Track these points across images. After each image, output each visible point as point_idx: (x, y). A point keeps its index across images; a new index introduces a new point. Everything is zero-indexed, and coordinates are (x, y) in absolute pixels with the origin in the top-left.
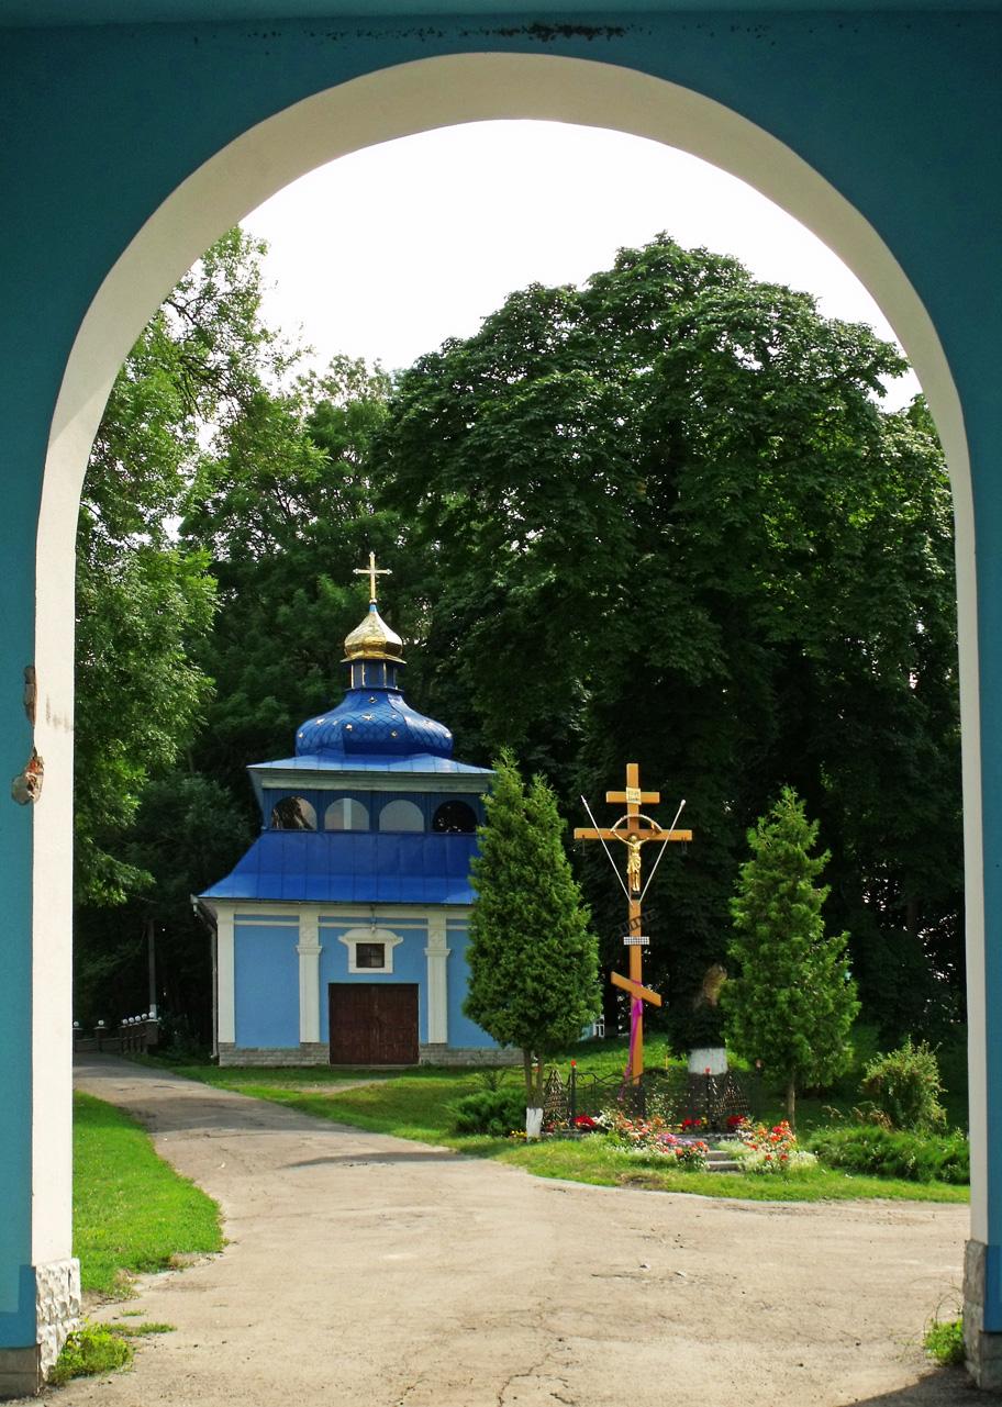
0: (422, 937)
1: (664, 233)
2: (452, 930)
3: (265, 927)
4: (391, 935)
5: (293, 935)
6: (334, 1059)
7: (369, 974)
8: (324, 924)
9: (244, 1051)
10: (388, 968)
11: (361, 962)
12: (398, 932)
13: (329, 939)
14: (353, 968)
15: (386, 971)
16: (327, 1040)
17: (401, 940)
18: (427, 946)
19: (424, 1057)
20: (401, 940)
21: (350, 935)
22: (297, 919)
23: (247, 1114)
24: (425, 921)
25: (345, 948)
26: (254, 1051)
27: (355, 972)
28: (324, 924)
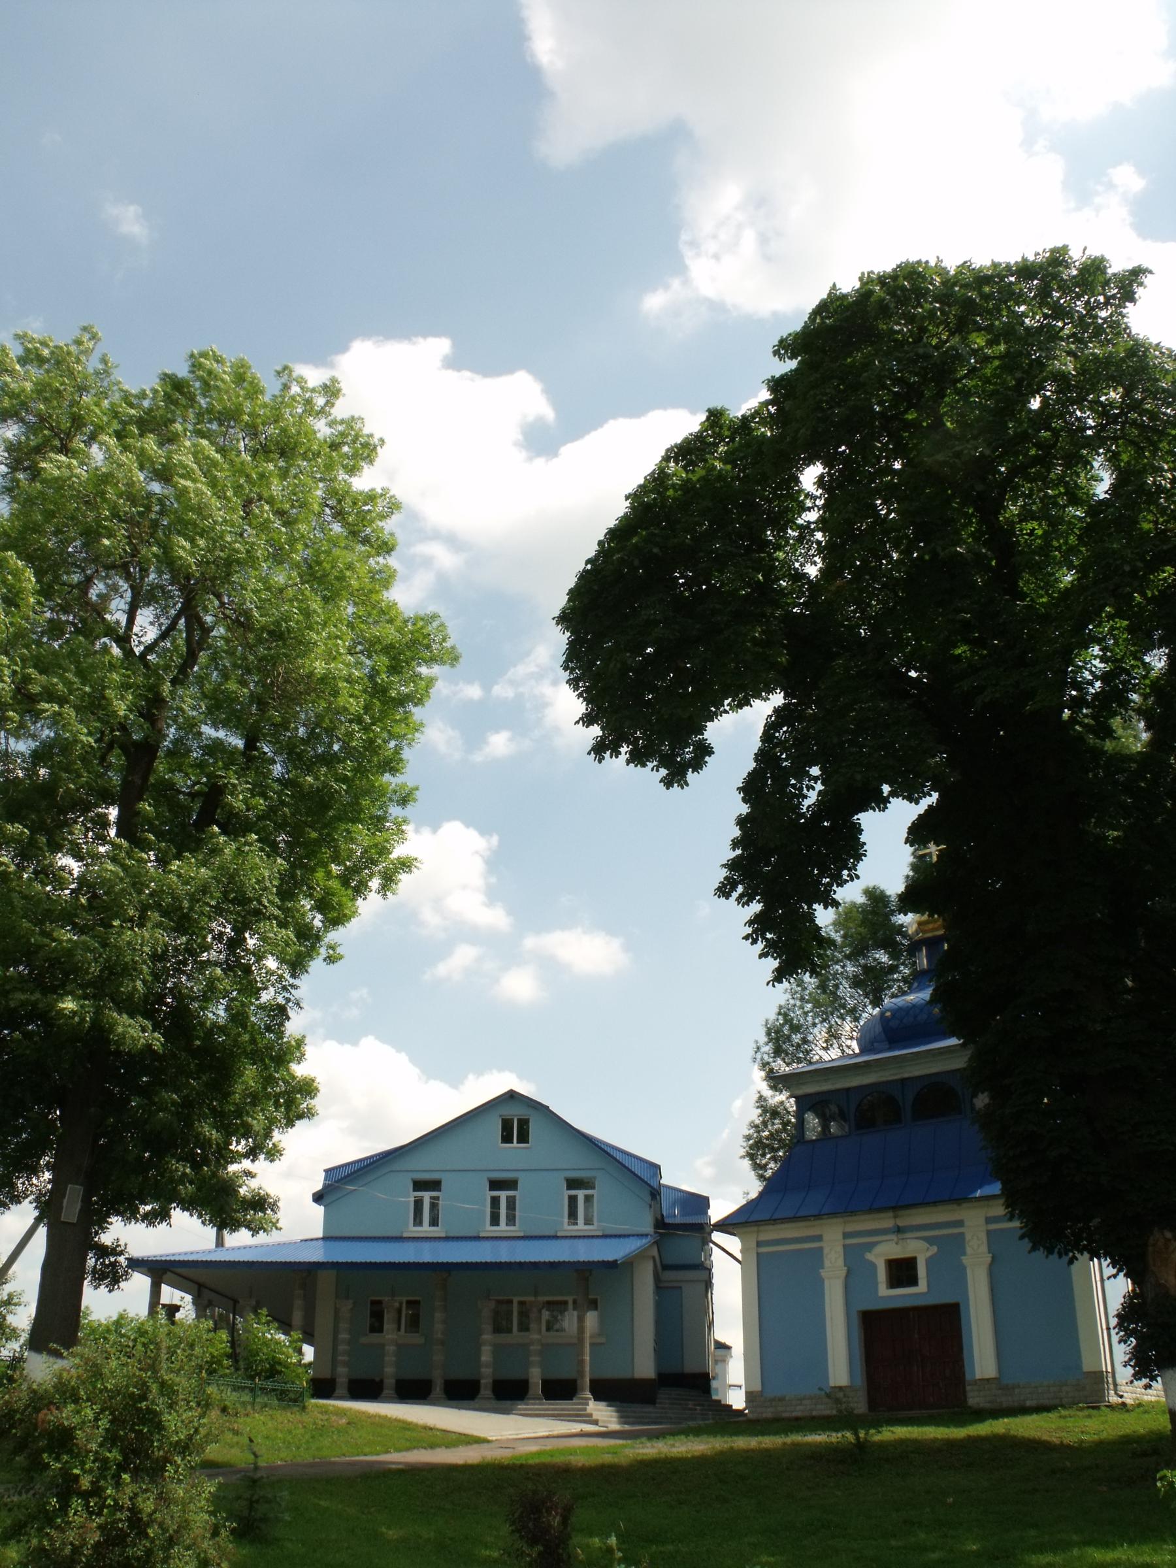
0: (959, 1243)
1: (746, 938)
2: (995, 1231)
3: (948, 1236)
4: (923, 1245)
5: (818, 1254)
6: (872, 1404)
7: (904, 1295)
8: (763, 1250)
9: (772, 1400)
10: (922, 1286)
11: (894, 1282)
12: (930, 1240)
13: (855, 1258)
14: (884, 1290)
15: (920, 1291)
16: (860, 1381)
17: (934, 1249)
18: (964, 1254)
19: (975, 1399)
20: (934, 1249)
21: (879, 1249)
22: (819, 1238)
23: (179, 1270)
24: (819, 1238)
25: (873, 1266)
26: (782, 1399)
27: (886, 1294)
28: (763, 1250)
